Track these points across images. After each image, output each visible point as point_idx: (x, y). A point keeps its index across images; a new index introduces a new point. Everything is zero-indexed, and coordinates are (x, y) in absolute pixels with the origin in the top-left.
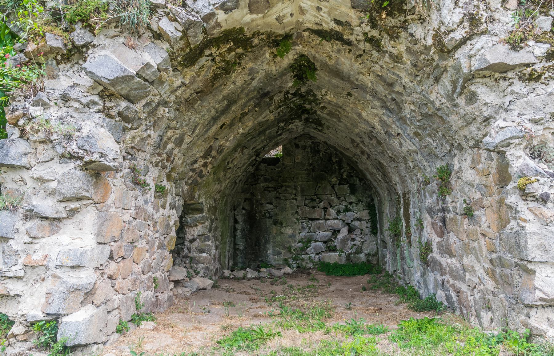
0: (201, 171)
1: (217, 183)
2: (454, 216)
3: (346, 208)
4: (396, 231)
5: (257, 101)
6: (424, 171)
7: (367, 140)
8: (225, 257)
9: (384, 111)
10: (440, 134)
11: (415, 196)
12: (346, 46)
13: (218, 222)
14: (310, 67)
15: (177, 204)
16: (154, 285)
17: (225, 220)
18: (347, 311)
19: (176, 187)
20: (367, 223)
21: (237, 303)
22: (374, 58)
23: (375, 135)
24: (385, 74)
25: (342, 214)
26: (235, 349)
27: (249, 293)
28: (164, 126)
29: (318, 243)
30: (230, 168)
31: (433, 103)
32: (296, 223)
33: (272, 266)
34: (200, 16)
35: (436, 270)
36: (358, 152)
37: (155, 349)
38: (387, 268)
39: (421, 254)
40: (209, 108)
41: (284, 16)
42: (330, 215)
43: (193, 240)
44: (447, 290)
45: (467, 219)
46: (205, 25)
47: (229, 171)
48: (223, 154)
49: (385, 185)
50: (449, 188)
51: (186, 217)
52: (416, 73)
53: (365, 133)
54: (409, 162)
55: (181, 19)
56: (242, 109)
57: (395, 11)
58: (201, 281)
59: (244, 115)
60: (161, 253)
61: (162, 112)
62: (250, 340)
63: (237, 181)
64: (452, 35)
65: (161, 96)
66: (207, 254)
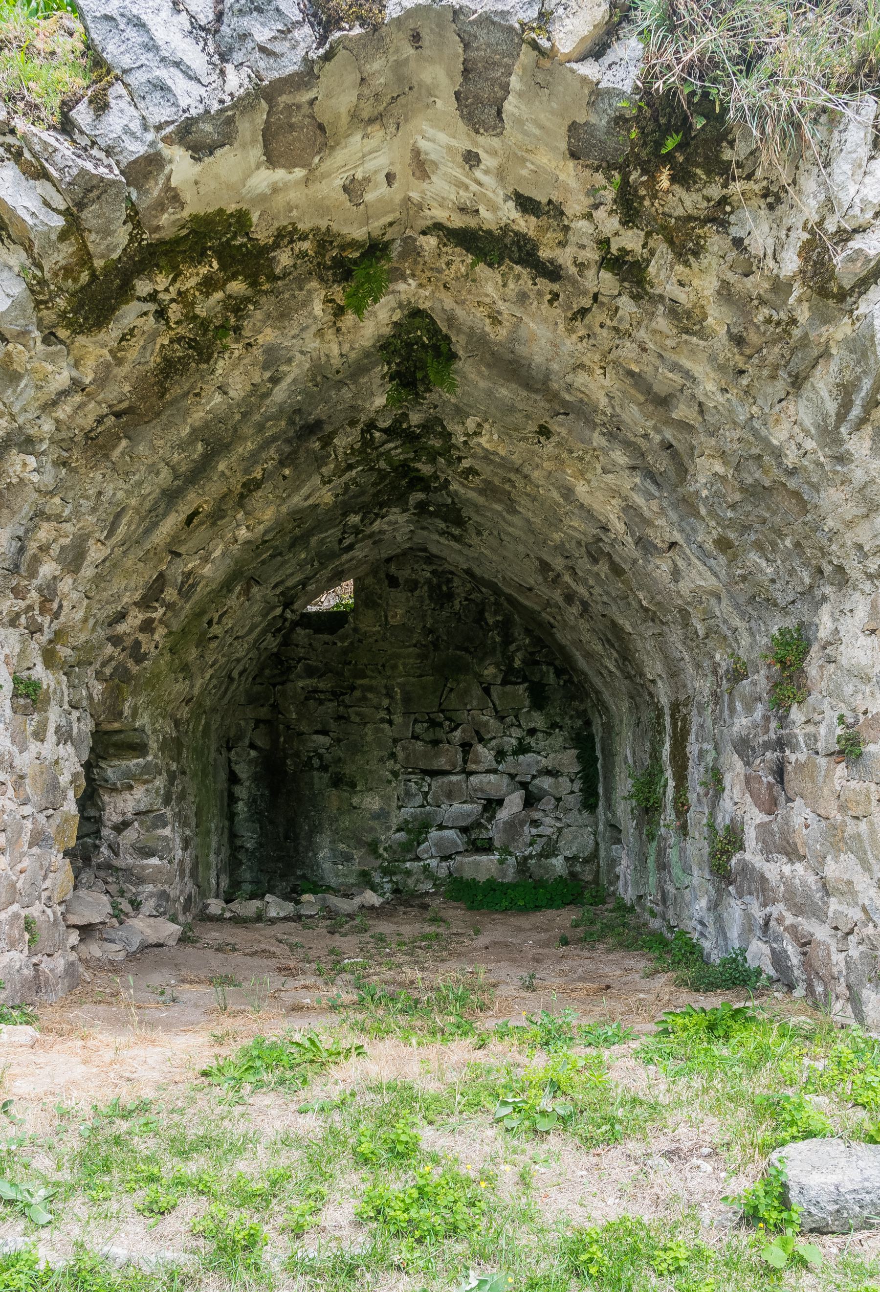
0: (137, 644)
1: (181, 676)
2: (808, 758)
3: (520, 743)
4: (647, 800)
5: (287, 449)
6: (735, 645)
7: (584, 564)
8: (208, 866)
9: (637, 480)
10: (788, 542)
11: (704, 709)
12: (545, 281)
13: (187, 779)
14: (436, 348)
15: (75, 731)
16: (27, 937)
17: (205, 774)
18: (524, 994)
19: (72, 686)
20: (572, 781)
21: (245, 979)
22: (621, 319)
23: (607, 549)
24: (649, 369)
25: (510, 759)
26: (248, 1087)
27: (273, 955)
28: (27, 510)
29: (447, 833)
30: (216, 637)
31: (778, 454)
32: (389, 782)
33: (329, 889)
34: (118, 163)
35: (750, 893)
36: (557, 596)
37: (40, 1090)
38: (621, 890)
39: (712, 855)
40: (154, 464)
41: (367, 180)
42: (477, 762)
43: (121, 827)
44: (777, 939)
45: (843, 764)
46: (134, 196)
47: (213, 645)
48: (195, 598)
49: (623, 685)
50: (799, 688)
51: (103, 764)
52: (741, 365)
53: (579, 543)
54: (694, 621)
55: (61, 170)
56: (247, 471)
57: (698, 165)
58: (150, 926)
59: (251, 486)
60: (39, 857)
61: (18, 468)
62: (287, 1066)
63: (235, 674)
64: (856, 243)
65: (13, 418)
66: (161, 858)
